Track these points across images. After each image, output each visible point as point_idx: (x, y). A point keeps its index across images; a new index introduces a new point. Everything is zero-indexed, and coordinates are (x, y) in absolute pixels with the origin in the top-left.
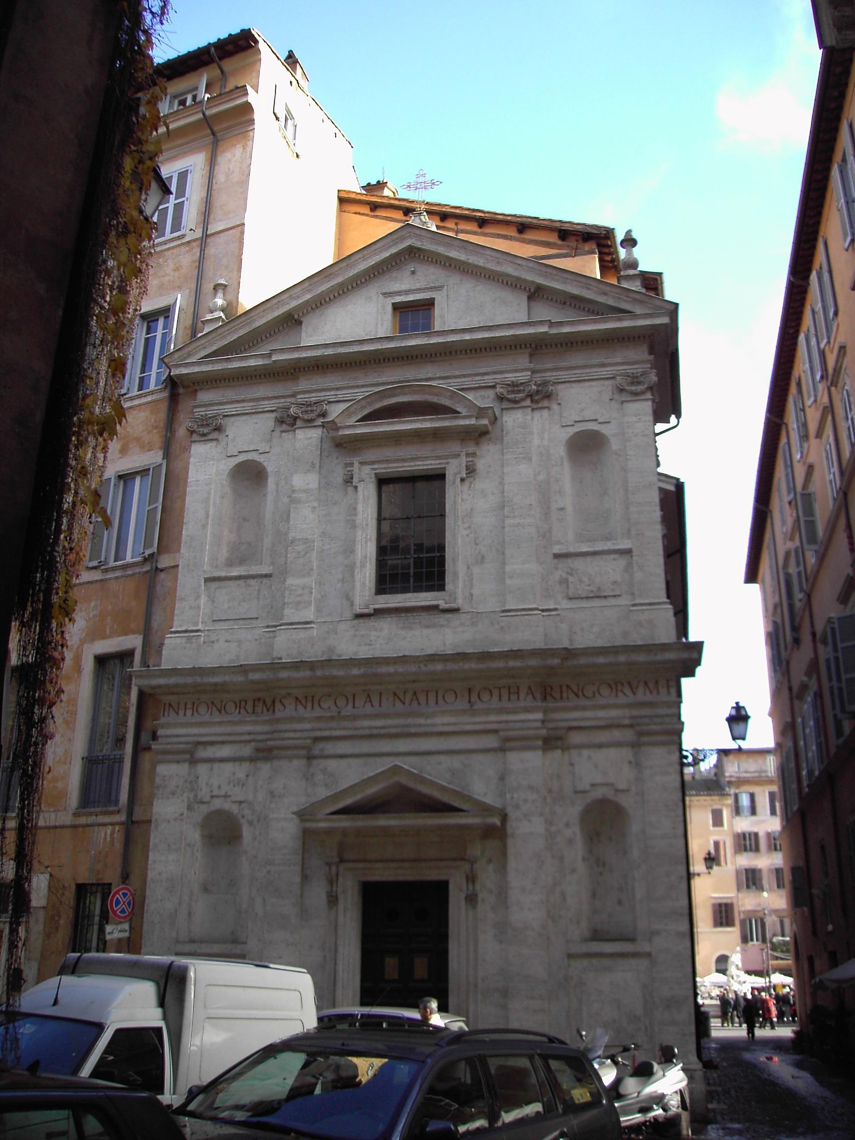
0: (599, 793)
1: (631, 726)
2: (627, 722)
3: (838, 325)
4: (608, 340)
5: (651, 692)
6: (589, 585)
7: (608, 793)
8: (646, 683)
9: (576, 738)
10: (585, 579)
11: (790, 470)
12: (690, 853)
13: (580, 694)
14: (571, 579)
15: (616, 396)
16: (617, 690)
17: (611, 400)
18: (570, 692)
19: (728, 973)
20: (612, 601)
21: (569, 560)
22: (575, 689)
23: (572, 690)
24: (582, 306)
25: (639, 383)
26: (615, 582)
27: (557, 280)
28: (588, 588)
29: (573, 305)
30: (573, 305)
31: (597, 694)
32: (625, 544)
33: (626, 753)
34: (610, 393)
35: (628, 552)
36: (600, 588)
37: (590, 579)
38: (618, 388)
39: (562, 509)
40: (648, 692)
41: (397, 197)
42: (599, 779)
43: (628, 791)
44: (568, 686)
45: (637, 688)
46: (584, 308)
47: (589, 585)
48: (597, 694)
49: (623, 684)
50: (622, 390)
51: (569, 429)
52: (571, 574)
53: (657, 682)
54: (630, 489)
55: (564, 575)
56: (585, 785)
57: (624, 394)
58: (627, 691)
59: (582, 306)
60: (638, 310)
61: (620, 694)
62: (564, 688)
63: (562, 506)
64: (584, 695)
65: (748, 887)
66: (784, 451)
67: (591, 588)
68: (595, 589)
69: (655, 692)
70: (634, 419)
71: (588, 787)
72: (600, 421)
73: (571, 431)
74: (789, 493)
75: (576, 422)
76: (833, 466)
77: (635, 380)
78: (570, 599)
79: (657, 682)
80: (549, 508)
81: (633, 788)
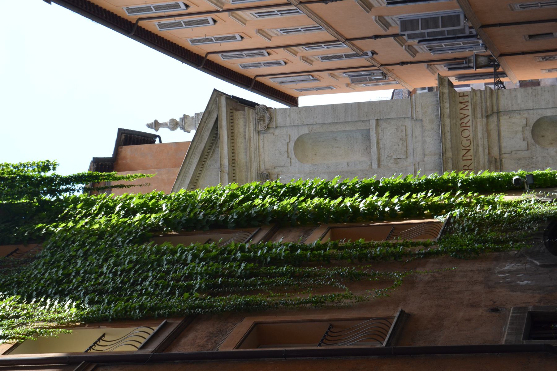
0: (528, 134)
4: (232, 136)
5: (467, 106)
6: (399, 146)
7: (529, 129)
9: (495, 152)
10: (394, 148)
11: (244, 53)
12: (463, 343)
13: (468, 148)
14: (394, 157)
17: (274, 134)
18: (466, 155)
21: (382, 159)
22: (466, 151)
23: (465, 154)
24: (206, 154)
26: (397, 129)
27: (189, 169)
28: (400, 146)
29: (205, 160)
30: (205, 160)
32: (373, 123)
33: (504, 120)
34: (269, 135)
35: (377, 120)
36: (401, 139)
37: (395, 145)
39: (348, 164)
42: (520, 136)
43: (526, 118)
44: (463, 156)
47: (399, 146)
51: (293, 161)
52: (392, 156)
55: (392, 161)
56: (524, 144)
58: (466, 120)
59: (206, 154)
60: (214, 116)
62: (465, 158)
63: (346, 164)
64: (469, 146)
66: (224, 57)
67: (400, 144)
68: (401, 142)
70: (288, 119)
71: (525, 142)
72: (288, 141)
73: (294, 160)
74: (262, 54)
75: (288, 157)
76: (274, 12)
78: (407, 157)
80: (347, 172)
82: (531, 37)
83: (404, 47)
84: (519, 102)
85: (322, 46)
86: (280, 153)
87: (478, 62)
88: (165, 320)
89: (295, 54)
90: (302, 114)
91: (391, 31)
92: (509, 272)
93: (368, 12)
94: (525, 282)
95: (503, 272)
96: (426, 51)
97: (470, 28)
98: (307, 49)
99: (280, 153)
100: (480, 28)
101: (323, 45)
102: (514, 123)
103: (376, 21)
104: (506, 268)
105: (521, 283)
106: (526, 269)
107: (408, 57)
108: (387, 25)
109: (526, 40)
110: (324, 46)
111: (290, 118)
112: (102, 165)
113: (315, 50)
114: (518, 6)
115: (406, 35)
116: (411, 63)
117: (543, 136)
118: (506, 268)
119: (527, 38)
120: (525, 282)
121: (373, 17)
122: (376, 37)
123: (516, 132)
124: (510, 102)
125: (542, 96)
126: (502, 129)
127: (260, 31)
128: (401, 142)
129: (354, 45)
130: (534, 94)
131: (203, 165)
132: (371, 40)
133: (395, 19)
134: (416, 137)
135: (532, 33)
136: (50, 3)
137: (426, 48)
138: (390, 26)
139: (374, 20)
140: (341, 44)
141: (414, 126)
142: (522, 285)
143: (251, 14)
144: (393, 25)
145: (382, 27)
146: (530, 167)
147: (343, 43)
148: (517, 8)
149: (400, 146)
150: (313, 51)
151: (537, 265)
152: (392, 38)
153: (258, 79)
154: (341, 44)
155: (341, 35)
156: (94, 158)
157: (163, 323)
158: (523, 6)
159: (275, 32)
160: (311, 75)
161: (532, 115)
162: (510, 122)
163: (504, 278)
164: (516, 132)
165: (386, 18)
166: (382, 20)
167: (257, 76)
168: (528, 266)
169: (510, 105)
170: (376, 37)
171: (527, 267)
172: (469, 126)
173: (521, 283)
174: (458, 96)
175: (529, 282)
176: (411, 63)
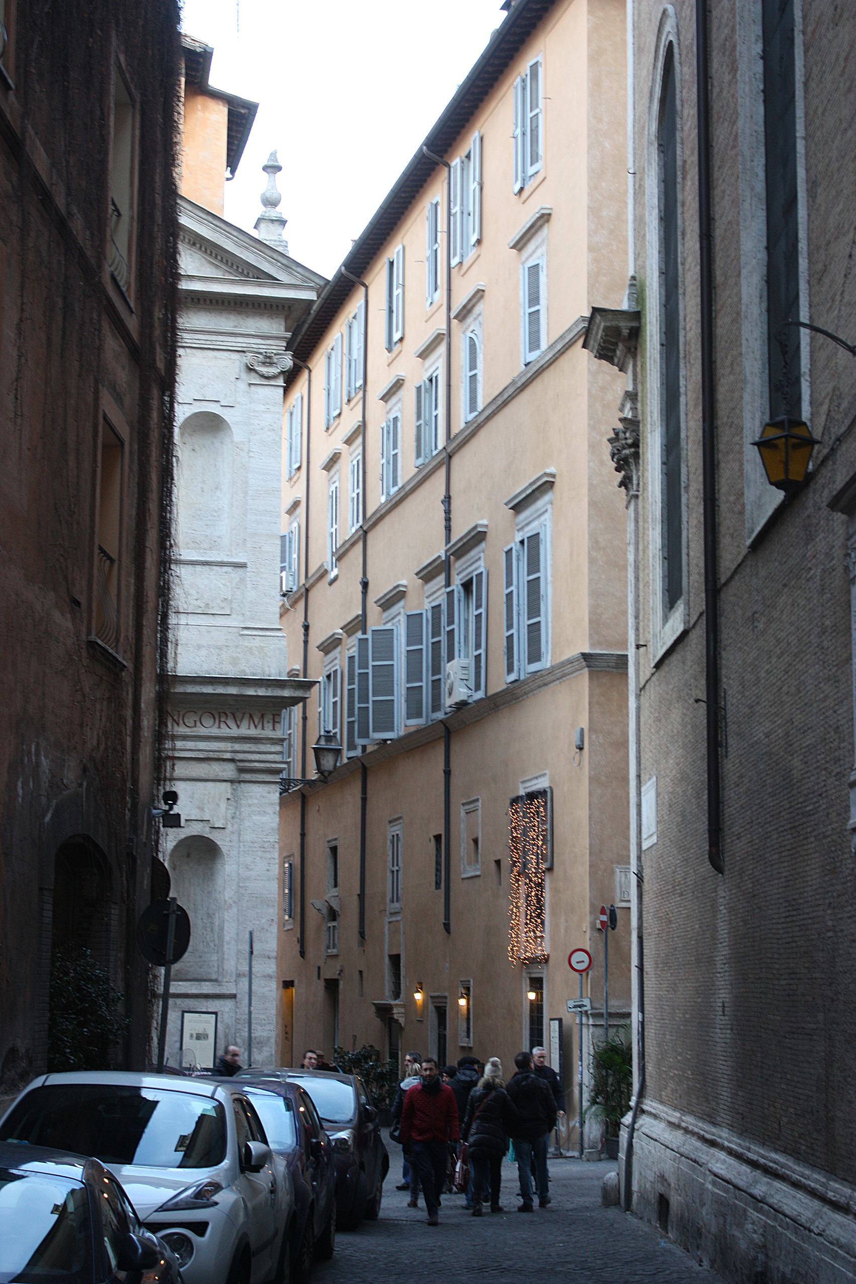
1: (232, 760)
2: (228, 756)
3: (401, 352)
4: (247, 305)
5: (256, 727)
8: (251, 716)
10: (193, 592)
15: (244, 375)
16: (220, 721)
19: (336, 977)
20: (220, 621)
25: (271, 364)
28: (195, 603)
31: (198, 724)
34: (237, 370)
38: (247, 367)
40: (252, 725)
41: (815, 324)
45: (241, 721)
46: (216, 255)
48: (198, 724)
49: (226, 715)
50: (250, 369)
53: (263, 716)
54: (250, 492)
57: (253, 374)
60: (283, 277)
61: (223, 725)
65: (235, 1100)
67: (199, 603)
68: (202, 605)
69: (260, 726)
70: (262, 408)
77: (268, 361)
79: (263, 716)
81: (229, 826)
82: (334, 850)
83: (341, 631)
84: (254, 818)
85: (358, 487)
86: (203, 387)
87: (326, 753)
88: (13, 86)
89: (349, 441)
90: (269, 433)
91: (373, 610)
92: (38, 764)
93: (417, 574)
94: (20, 792)
95: (38, 754)
96: (327, 668)
97: (364, 748)
98: (355, 462)
99: (203, 387)
100: (363, 764)
101: (360, 491)
102: (218, 805)
103: (398, 586)
104: (43, 758)
105: (20, 784)
106: (41, 795)
107: (318, 636)
108: (387, 603)
109: (329, 842)
110: (356, 491)
111: (263, 412)
112: (198, 63)
113: (350, 476)
114: (398, 832)
115: (364, 637)
116: (306, 642)
117: (188, 855)
118: (43, 758)
119: (333, 844)
120: (20, 792)
121: (404, 582)
122: (365, 585)
123: (201, 809)
124: (255, 801)
125: (261, 858)
126: (210, 785)
127: (398, 385)
128: (202, 605)
129: (353, 544)
130: (266, 845)
131: (194, 244)
132: (361, 576)
133: (397, 619)
134: (209, 632)
135: (339, 851)
136: (503, 8)
137: (334, 669)
138: (384, 611)
139: (400, 583)
140: (358, 522)
141: (230, 630)
142: (16, 785)
143: (437, 368)
144: (385, 614)
145: (385, 595)
146: (746, 780)
147: (361, 527)
148: (393, 829)
149: (195, 603)
150: (350, 472)
151: (44, 817)
152: (360, 612)
153: (306, 372)
154: (358, 522)
155: (375, 524)
156: (211, 54)
157: (10, 81)
158: (395, 839)
159: (396, 408)
160: (299, 468)
161: (228, 839)
162: (220, 800)
163: (30, 752)
164: (201, 809)
165: (402, 603)
166: (396, 596)
167: (310, 371)
168: (44, 800)
169: (250, 802)
170: (365, 585)
171: (42, 797)
172: (219, 727)
173: (20, 784)
174: (274, 713)
175: (20, 800)
176: (306, 642)
